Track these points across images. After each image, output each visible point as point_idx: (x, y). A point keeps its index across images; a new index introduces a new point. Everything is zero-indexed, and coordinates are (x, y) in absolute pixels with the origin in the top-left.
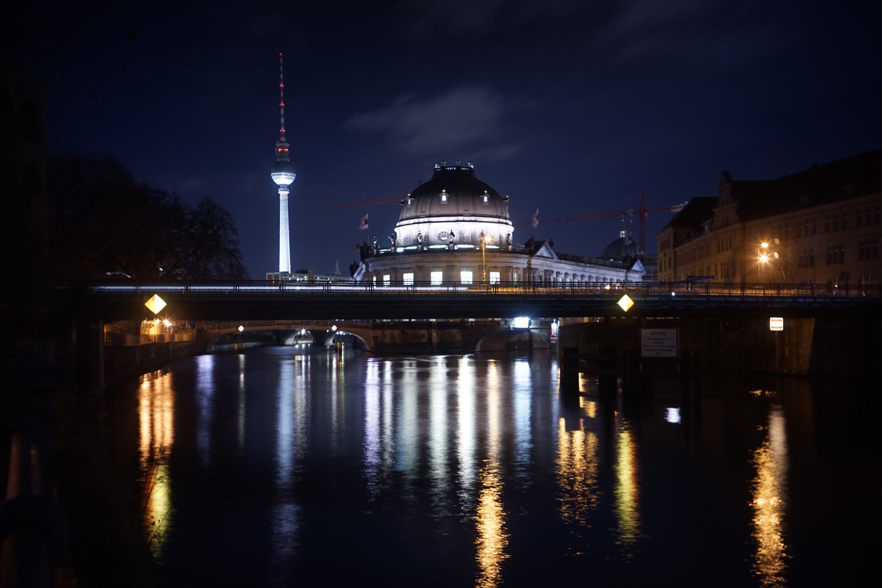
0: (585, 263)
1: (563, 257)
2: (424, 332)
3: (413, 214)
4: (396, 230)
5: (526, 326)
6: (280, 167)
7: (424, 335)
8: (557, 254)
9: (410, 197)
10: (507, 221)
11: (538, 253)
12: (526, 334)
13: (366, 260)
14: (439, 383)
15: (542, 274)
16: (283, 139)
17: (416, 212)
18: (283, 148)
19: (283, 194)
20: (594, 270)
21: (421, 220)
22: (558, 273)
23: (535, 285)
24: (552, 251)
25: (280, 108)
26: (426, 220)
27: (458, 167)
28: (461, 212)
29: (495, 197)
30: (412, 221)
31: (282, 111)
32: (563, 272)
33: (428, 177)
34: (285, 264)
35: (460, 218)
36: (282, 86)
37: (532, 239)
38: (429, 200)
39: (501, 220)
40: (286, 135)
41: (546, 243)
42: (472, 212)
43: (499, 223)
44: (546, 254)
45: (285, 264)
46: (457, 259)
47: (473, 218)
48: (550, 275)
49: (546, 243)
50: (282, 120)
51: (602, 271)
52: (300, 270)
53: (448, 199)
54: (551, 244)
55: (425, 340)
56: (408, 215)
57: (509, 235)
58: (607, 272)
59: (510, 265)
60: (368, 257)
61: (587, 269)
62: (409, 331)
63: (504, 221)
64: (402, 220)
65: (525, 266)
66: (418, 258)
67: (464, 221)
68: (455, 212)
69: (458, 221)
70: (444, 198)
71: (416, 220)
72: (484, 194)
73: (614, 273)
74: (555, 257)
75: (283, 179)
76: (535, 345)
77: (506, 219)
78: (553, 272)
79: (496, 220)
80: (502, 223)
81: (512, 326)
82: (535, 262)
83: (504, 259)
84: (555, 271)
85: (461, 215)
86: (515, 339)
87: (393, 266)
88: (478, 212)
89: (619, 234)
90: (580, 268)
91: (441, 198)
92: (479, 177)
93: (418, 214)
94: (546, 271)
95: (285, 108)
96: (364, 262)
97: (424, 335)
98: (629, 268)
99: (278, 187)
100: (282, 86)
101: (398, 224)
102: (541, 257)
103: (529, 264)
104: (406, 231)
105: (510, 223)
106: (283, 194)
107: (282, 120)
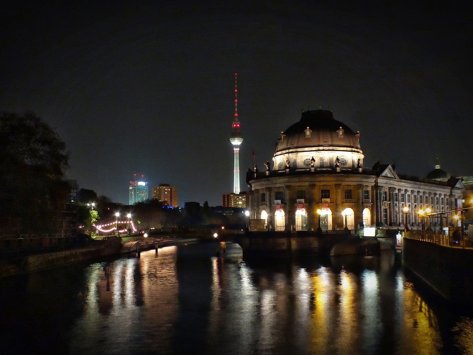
0: (421, 182)
1: (403, 177)
3: (284, 146)
5: (374, 236)
6: (235, 135)
7: (284, 244)
8: (398, 175)
9: (283, 134)
10: (358, 150)
11: (384, 174)
13: (250, 182)
14: (267, 311)
15: (387, 190)
16: (237, 120)
17: (287, 145)
19: (236, 150)
20: (427, 187)
21: (291, 150)
22: (399, 190)
23: (324, 167)
26: (294, 150)
28: (321, 144)
29: (349, 132)
30: (284, 152)
32: (404, 189)
35: (321, 148)
36: (236, 91)
39: (354, 149)
41: (390, 166)
42: (330, 143)
43: (352, 151)
44: (389, 175)
46: (317, 179)
47: (331, 148)
48: (393, 191)
49: (390, 166)
53: (312, 134)
54: (394, 167)
55: (285, 247)
57: (359, 160)
58: (437, 189)
59: (360, 183)
61: (422, 187)
63: (356, 150)
65: (373, 184)
66: (286, 179)
67: (323, 150)
70: (308, 133)
71: (287, 151)
72: (339, 129)
73: (442, 190)
74: (397, 177)
75: (236, 142)
76: (382, 247)
77: (357, 148)
78: (395, 189)
80: (354, 151)
82: (381, 181)
83: (356, 179)
84: (397, 188)
86: (366, 243)
87: (268, 186)
88: (335, 143)
90: (416, 186)
91: (305, 134)
92: (337, 117)
93: (289, 146)
94: (390, 188)
95: (237, 103)
97: (284, 244)
100: (236, 91)
102: (386, 177)
103: (376, 182)
104: (279, 160)
105: (361, 152)
106: (236, 150)
107: (236, 109)
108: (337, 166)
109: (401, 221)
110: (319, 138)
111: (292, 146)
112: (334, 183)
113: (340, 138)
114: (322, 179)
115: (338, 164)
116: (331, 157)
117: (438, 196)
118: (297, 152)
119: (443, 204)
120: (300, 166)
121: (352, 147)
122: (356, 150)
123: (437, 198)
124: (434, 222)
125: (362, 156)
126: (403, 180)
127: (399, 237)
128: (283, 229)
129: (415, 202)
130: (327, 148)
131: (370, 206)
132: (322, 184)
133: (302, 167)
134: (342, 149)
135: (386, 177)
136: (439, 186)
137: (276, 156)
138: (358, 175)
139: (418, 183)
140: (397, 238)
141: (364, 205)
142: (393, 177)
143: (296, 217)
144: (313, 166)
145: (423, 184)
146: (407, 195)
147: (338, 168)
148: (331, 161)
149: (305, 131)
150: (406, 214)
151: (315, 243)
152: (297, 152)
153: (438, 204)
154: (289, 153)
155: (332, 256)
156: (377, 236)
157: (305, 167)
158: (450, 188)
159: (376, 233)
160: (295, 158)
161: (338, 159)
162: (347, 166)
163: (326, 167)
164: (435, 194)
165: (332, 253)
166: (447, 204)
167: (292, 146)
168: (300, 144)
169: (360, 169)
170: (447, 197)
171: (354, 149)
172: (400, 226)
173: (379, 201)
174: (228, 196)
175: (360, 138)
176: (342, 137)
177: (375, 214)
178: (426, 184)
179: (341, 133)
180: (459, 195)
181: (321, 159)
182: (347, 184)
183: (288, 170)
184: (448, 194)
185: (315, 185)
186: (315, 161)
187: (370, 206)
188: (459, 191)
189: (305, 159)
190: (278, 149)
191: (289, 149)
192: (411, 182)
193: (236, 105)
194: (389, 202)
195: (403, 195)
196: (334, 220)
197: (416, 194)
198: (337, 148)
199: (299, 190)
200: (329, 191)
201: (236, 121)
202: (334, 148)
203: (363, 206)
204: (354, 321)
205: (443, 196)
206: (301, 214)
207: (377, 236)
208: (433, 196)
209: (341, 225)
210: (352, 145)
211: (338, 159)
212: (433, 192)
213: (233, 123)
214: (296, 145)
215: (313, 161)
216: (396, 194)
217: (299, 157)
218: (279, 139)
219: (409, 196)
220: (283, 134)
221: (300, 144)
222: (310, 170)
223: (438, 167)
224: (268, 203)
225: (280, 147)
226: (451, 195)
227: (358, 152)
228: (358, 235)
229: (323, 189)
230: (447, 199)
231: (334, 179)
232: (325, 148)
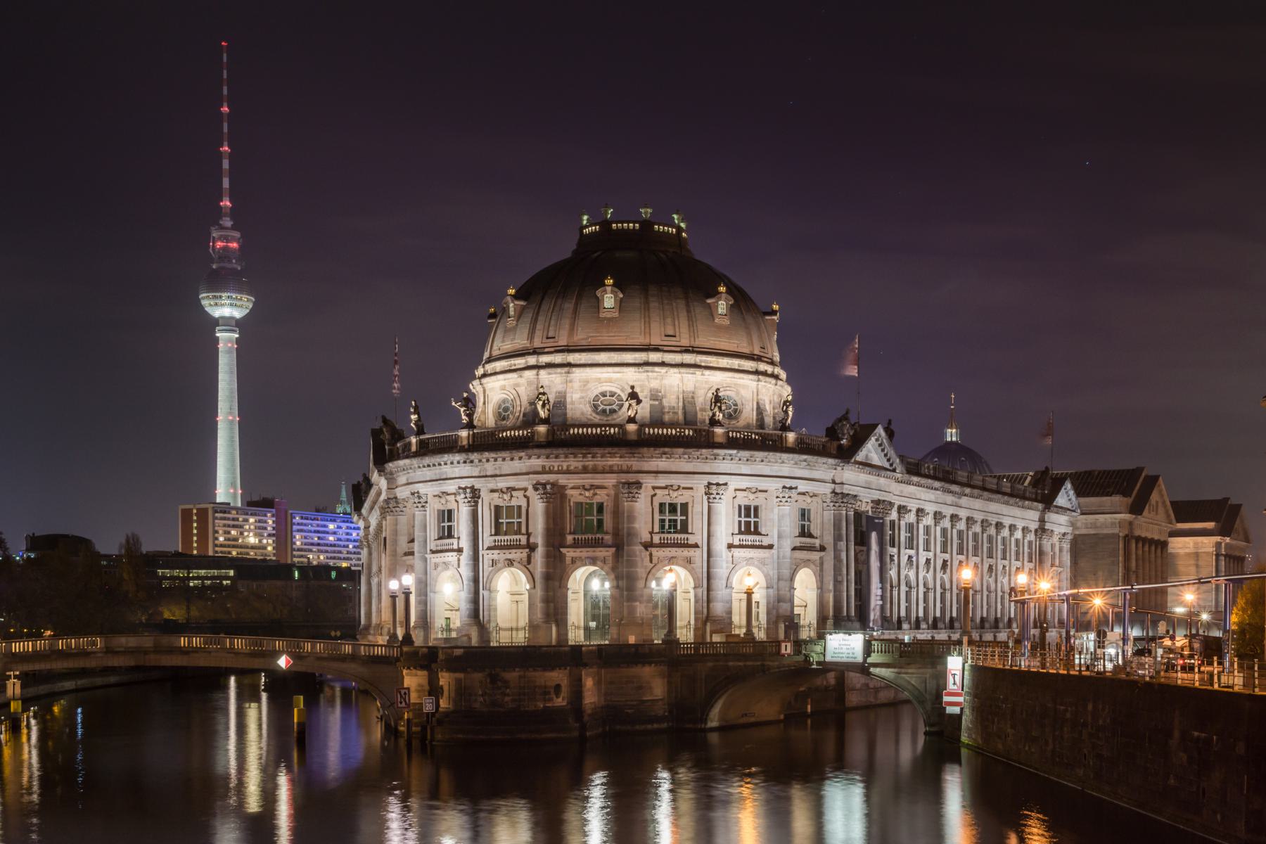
2: (558, 676)
3: (521, 341)
4: (475, 387)
5: (860, 659)
6: (219, 281)
7: (558, 688)
9: (515, 297)
11: (860, 456)
12: (831, 678)
13: (390, 466)
16: (228, 222)
17: (531, 336)
18: (225, 241)
19: (226, 339)
20: (978, 504)
21: (545, 359)
22: (902, 510)
23: (662, 425)
24: (892, 453)
25: (220, 156)
26: (558, 358)
27: (647, 224)
28: (656, 340)
29: (743, 303)
30: (520, 362)
31: (226, 164)
33: (565, 250)
34: (226, 488)
35: (654, 357)
36: (225, 109)
37: (845, 417)
38: (569, 306)
40: (234, 213)
41: (880, 430)
42: (685, 342)
43: (757, 372)
44: (876, 459)
45: (226, 488)
47: (689, 358)
49: (880, 430)
50: (226, 183)
51: (994, 507)
52: (256, 498)
53: (621, 305)
54: (890, 434)
55: (560, 702)
56: (508, 346)
58: (1004, 509)
60: (394, 456)
61: (964, 501)
62: (512, 676)
63: (769, 369)
64: (490, 360)
66: (536, 463)
67: (663, 364)
68: (640, 340)
71: (532, 360)
75: (227, 308)
77: (772, 363)
78: (891, 504)
79: (749, 365)
80: (765, 374)
81: (815, 658)
85: (656, 349)
88: (703, 341)
89: (944, 435)
90: (950, 498)
91: (598, 302)
92: (702, 253)
93: (537, 343)
94: (877, 502)
96: (381, 471)
97: (558, 688)
98: (1047, 501)
99: (215, 322)
100: (225, 109)
101: (480, 371)
102: (866, 465)
106: (226, 339)
108: (714, 422)
109: (903, 613)
110: (648, 323)
111: (550, 343)
113: (720, 327)
114: (662, 464)
115: (720, 416)
116: (689, 387)
117: (1006, 533)
118: (569, 365)
119: (1017, 559)
120: (578, 415)
121: (758, 359)
122: (769, 369)
123: (1004, 539)
124: (992, 617)
125: (786, 391)
126: (915, 479)
127: (955, 664)
128: (520, 638)
129: (944, 551)
130: (677, 358)
132: (663, 481)
133: (584, 420)
135: (866, 465)
136: (1012, 500)
137: (485, 375)
139: (955, 488)
140: (949, 666)
142: (887, 465)
143: (570, 595)
144: (631, 420)
145: (968, 490)
146: (921, 526)
147: (719, 431)
148: (688, 401)
149: (598, 293)
150: (967, 590)
151: (656, 686)
153: (1004, 558)
154: (537, 367)
155: (712, 730)
156: (870, 660)
157: (597, 419)
158: (1040, 506)
159: (868, 650)
160: (560, 388)
161: (717, 399)
162: (742, 422)
163: (672, 425)
164: (999, 526)
165: (714, 719)
166: (1030, 561)
167: (550, 343)
168: (583, 335)
169: (791, 437)
170: (1031, 537)
171: (763, 367)
172: (900, 628)
174: (203, 514)
175: (780, 328)
176: (727, 322)
178: (976, 492)
179: (722, 306)
180: (1063, 530)
181: (655, 396)
183: (542, 429)
184: (1034, 526)
186: (639, 402)
187: (814, 562)
189: (596, 392)
190: (496, 353)
191: (536, 352)
192: (937, 484)
193: (226, 164)
195: (910, 527)
197: (946, 523)
198: (704, 358)
199: (581, 499)
200: (685, 507)
201: (222, 228)
202: (700, 359)
205: (1018, 535)
206: (589, 583)
207: (870, 660)
208: (992, 531)
209: (724, 624)
211: (717, 399)
212: (993, 520)
213: (215, 234)
215: (633, 402)
216: (892, 523)
217: (576, 385)
218: (493, 316)
219: (927, 528)
220: (515, 297)
222: (625, 432)
223: (952, 435)
224: (465, 543)
225: (500, 344)
226: (1042, 530)
227: (776, 377)
228: (806, 656)
229: (667, 500)
230: (1030, 543)
232: (669, 358)
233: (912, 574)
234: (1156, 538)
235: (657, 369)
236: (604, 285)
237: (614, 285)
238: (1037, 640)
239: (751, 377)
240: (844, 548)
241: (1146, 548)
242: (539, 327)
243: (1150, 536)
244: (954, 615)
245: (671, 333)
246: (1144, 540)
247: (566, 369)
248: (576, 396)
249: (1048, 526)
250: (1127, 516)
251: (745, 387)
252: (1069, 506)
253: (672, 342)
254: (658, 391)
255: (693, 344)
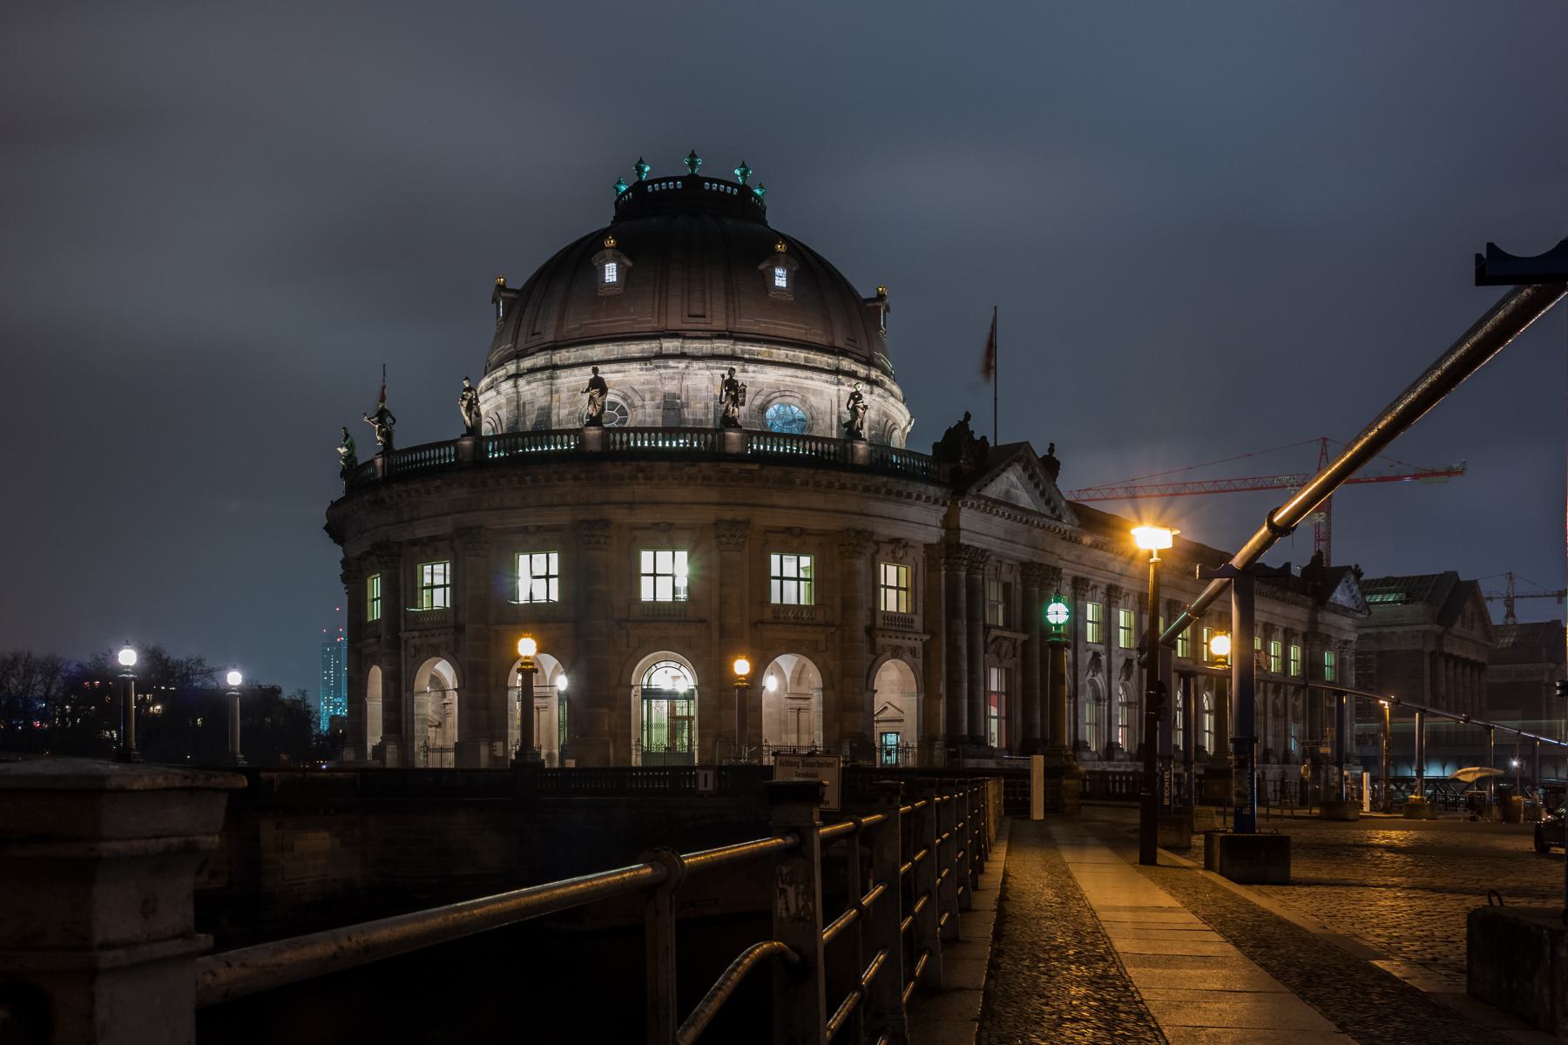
11: (994, 490)
17: (515, 340)
28: (674, 323)
35: (670, 345)
42: (719, 324)
43: (837, 371)
65: (934, 535)
67: (682, 356)
68: (651, 324)
69: (661, 356)
85: (674, 335)
102: (1006, 505)
103: (951, 526)
112: (709, 515)
114: (641, 490)
118: (555, 367)
121: (844, 353)
131: (913, 651)
134: (781, 353)
138: (846, 477)
141: (880, 641)
150: (742, 689)
152: (555, 367)
158: (1310, 601)
160: (543, 401)
167: (536, 340)
168: (572, 327)
173: (962, 624)
177: (942, 690)
182: (783, 522)
185: (606, 523)
187: (913, 651)
188: (1346, 622)
194: (1022, 637)
196: (580, 708)
203: (873, 650)
204: (1163, 511)
210: (839, 343)
214: (549, 337)
217: (564, 396)
221: (572, 327)
231: (713, 495)
232: (693, 346)
233: (1100, 679)
234: (1472, 657)
235: (671, 363)
236: (604, 247)
237: (618, 247)
238: (1322, 529)
239: (825, 376)
240: (965, 629)
241: (1459, 670)
242: (524, 322)
243: (1464, 655)
244: (1270, 746)
245: (699, 312)
246: (1458, 660)
247: (547, 373)
248: (564, 412)
249: (1322, 629)
250: (1437, 628)
251: (816, 392)
252: (1353, 606)
253: (700, 324)
254: (674, 396)
255: (731, 327)
